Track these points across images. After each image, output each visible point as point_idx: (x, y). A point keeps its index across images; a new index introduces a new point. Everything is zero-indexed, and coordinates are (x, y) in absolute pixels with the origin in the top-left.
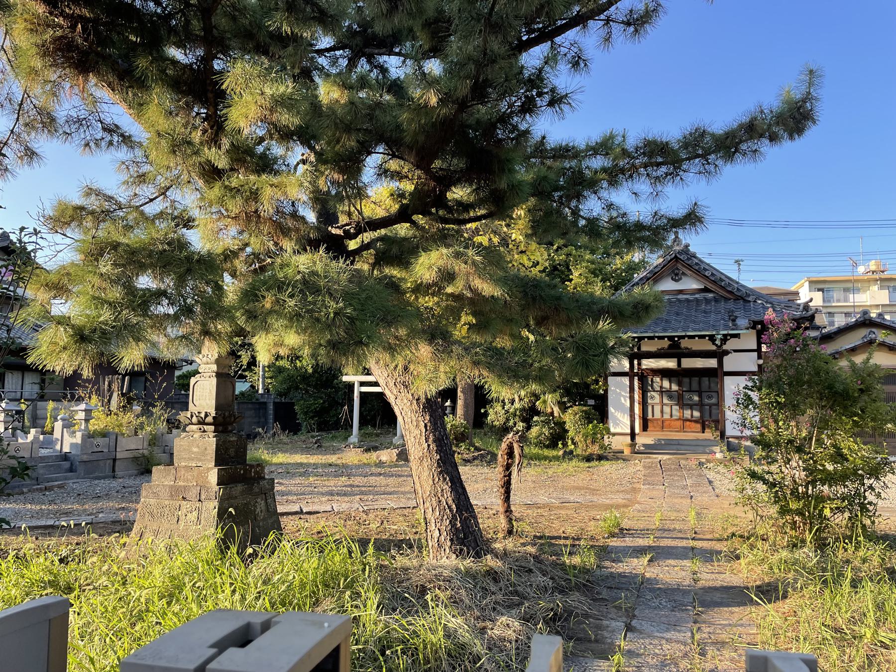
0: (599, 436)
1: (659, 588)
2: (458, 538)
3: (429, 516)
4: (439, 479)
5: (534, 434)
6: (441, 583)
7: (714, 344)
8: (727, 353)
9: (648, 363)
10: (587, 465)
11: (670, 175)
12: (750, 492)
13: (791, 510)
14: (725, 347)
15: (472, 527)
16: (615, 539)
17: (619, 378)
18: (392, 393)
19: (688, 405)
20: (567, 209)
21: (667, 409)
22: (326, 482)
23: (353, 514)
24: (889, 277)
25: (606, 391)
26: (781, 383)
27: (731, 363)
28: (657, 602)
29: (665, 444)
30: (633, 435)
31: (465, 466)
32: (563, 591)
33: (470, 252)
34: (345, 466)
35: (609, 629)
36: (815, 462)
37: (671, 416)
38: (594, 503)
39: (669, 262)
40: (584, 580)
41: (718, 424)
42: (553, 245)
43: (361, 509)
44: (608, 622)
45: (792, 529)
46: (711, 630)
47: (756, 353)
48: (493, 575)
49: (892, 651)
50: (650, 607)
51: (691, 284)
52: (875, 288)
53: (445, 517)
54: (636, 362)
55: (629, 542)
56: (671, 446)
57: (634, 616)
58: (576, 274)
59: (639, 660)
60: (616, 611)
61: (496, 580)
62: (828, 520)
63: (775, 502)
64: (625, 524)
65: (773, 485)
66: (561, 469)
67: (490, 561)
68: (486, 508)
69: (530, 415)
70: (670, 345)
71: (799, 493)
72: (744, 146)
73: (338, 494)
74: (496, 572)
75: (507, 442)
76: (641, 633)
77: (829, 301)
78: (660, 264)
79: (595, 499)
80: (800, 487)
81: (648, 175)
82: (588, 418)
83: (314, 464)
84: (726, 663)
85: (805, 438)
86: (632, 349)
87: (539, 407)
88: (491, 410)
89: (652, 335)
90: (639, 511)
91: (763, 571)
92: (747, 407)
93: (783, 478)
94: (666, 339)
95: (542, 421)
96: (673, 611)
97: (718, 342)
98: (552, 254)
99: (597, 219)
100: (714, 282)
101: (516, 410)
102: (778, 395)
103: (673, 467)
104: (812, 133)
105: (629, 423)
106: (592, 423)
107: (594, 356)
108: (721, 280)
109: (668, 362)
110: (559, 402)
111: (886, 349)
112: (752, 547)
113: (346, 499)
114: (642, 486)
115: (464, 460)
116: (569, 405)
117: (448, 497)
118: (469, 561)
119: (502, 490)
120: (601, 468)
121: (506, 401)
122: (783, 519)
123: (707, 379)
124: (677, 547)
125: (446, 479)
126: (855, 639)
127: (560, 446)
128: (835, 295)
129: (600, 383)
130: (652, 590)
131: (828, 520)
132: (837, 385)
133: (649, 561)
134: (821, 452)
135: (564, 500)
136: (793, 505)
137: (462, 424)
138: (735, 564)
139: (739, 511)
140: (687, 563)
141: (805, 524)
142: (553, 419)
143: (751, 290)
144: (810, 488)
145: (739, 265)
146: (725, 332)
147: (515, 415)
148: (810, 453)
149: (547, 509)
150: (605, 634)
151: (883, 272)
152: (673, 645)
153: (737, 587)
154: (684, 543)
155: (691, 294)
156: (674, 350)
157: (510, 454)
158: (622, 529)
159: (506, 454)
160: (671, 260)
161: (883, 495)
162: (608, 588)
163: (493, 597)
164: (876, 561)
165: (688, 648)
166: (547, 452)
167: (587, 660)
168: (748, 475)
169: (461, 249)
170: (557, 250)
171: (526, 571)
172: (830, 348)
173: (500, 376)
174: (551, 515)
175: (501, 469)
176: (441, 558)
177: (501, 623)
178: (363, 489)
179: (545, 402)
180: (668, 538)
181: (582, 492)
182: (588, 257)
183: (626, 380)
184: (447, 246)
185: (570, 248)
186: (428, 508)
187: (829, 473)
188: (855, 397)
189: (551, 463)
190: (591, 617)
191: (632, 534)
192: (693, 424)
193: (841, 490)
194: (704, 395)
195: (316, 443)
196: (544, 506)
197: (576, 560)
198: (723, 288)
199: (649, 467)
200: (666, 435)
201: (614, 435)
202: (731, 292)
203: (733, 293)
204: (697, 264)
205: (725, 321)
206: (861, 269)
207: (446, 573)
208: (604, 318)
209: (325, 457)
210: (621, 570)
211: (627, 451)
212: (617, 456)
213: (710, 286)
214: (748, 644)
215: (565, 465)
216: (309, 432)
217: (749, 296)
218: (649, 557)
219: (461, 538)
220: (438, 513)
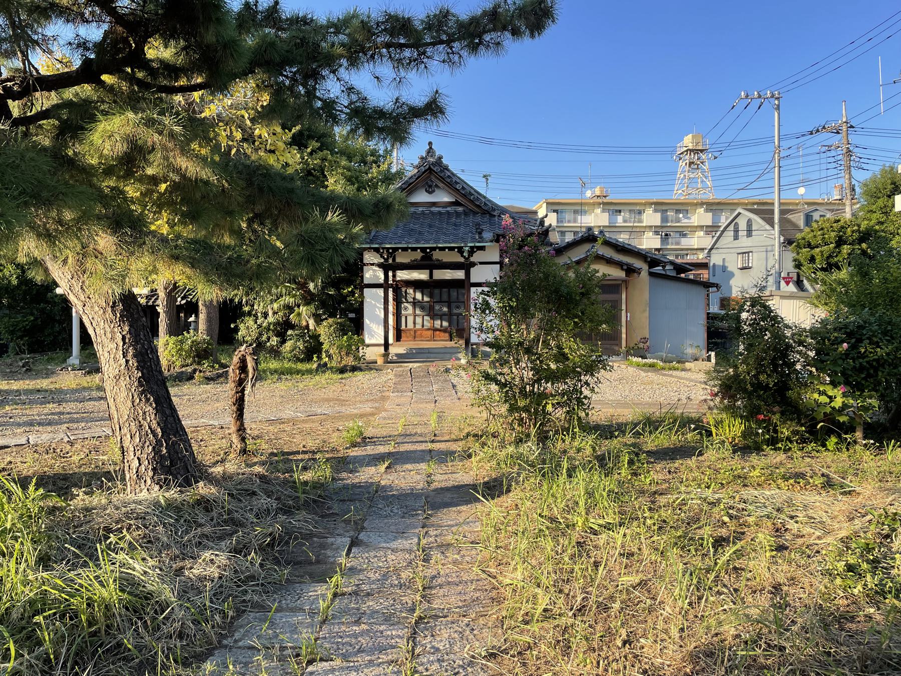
0: (353, 347)
1: (393, 495)
2: (163, 466)
3: (126, 443)
4: (140, 400)
5: (288, 349)
6: (132, 522)
7: (462, 256)
8: (473, 264)
9: (402, 275)
10: (340, 376)
11: (415, 61)
12: (484, 392)
13: (519, 407)
14: (472, 259)
15: (182, 452)
16: (357, 449)
17: (374, 290)
18: (79, 299)
19: (437, 315)
20: (301, 88)
21: (419, 320)
22: (27, 412)
23: (54, 445)
24: (610, 201)
25: (362, 303)
26: (514, 288)
27: (480, 274)
28: (388, 509)
29: (416, 353)
30: (386, 345)
31: (207, 384)
32: (289, 511)
33: (167, 120)
34: (60, 391)
35: (334, 546)
36: (541, 362)
37: (423, 326)
38: (341, 414)
39: (424, 173)
40: (315, 495)
41: (460, 331)
42: (307, 148)
43: (66, 439)
44: (333, 539)
45: (519, 425)
46: (437, 532)
47: (498, 266)
48: (205, 504)
49: (599, 536)
50: (381, 516)
51: (443, 197)
52: (598, 211)
53: (148, 443)
54: (390, 274)
55: (370, 450)
56: (422, 355)
57: (363, 528)
58: (331, 180)
59: (361, 577)
60: (344, 525)
61: (207, 510)
62: (550, 414)
63: (506, 401)
64: (370, 431)
65: (505, 385)
66: (313, 382)
67: (203, 489)
68: (222, 428)
69: (285, 329)
70: (422, 257)
71: (526, 392)
72: (487, 37)
73: (39, 424)
74: (208, 500)
75: (240, 355)
76: (367, 546)
77: (562, 222)
78: (415, 175)
79: (343, 409)
80: (528, 386)
81: (390, 57)
82: (342, 330)
83: (17, 391)
84: (449, 566)
85: (533, 340)
86: (386, 260)
87: (293, 321)
88: (242, 325)
89: (405, 246)
90: (385, 418)
91: (491, 467)
92: (483, 311)
93: (514, 378)
94: (419, 250)
95: (296, 335)
96: (403, 517)
97: (466, 254)
98: (306, 158)
99: (334, 102)
100: (464, 196)
101: (269, 324)
102: (510, 299)
103: (422, 374)
104: (551, 31)
105: (383, 334)
106: (346, 334)
107: (322, 250)
108: (471, 194)
109: (420, 274)
110: (314, 315)
111: (604, 262)
112: (484, 444)
113: (49, 428)
114: (391, 394)
115: (206, 378)
116: (324, 317)
117: (152, 419)
118: (173, 492)
119: (234, 408)
120: (354, 379)
121: (259, 314)
122: (512, 416)
123: (456, 290)
124: (415, 451)
125: (149, 399)
126: (568, 528)
127: (315, 359)
128: (568, 216)
129: (356, 295)
130: (385, 498)
131: (550, 414)
132: (563, 288)
133: (387, 468)
134: (547, 353)
135: (310, 413)
136: (521, 403)
137: (204, 340)
138: (467, 463)
139: (474, 412)
140: (423, 466)
141: (530, 420)
142: (308, 332)
143: (500, 206)
144: (536, 386)
145: (487, 179)
146: (472, 245)
147: (268, 329)
148: (536, 354)
149: (291, 424)
150: (329, 553)
151: (605, 197)
152: (397, 554)
153: (467, 485)
154: (423, 447)
155: (443, 207)
156: (427, 262)
157: (243, 368)
158: (365, 438)
159: (238, 368)
160: (425, 171)
161: (596, 390)
162: (341, 501)
163: (199, 529)
164: (589, 451)
165: (412, 557)
166: (300, 366)
167: (303, 586)
168: (483, 377)
169: (155, 116)
170: (311, 154)
171: (248, 494)
172: (562, 260)
173: (206, 274)
174: (294, 429)
175: (233, 385)
176: (141, 491)
177: (204, 560)
178: (75, 416)
179: (299, 314)
180: (408, 443)
181: (331, 404)
182: (344, 163)
183: (380, 292)
184: (135, 110)
185: (325, 152)
186: (125, 435)
187: (553, 372)
188: (576, 300)
189: (304, 377)
190: (315, 536)
191: (374, 442)
192: (442, 334)
193: (562, 387)
194: (453, 305)
195: (23, 366)
196: (289, 421)
197: (307, 476)
198: (472, 202)
199: (400, 376)
200: (418, 344)
201: (368, 346)
202: (478, 206)
203: (480, 207)
204: (449, 177)
205: (473, 234)
206: (589, 194)
207: (141, 509)
208: (333, 208)
209: (34, 382)
210: (357, 480)
211: (380, 361)
212: (371, 366)
213: (461, 199)
214: (472, 543)
215: (317, 377)
216: (17, 354)
217: (494, 210)
218: (387, 464)
219: (167, 466)
220: (138, 440)
